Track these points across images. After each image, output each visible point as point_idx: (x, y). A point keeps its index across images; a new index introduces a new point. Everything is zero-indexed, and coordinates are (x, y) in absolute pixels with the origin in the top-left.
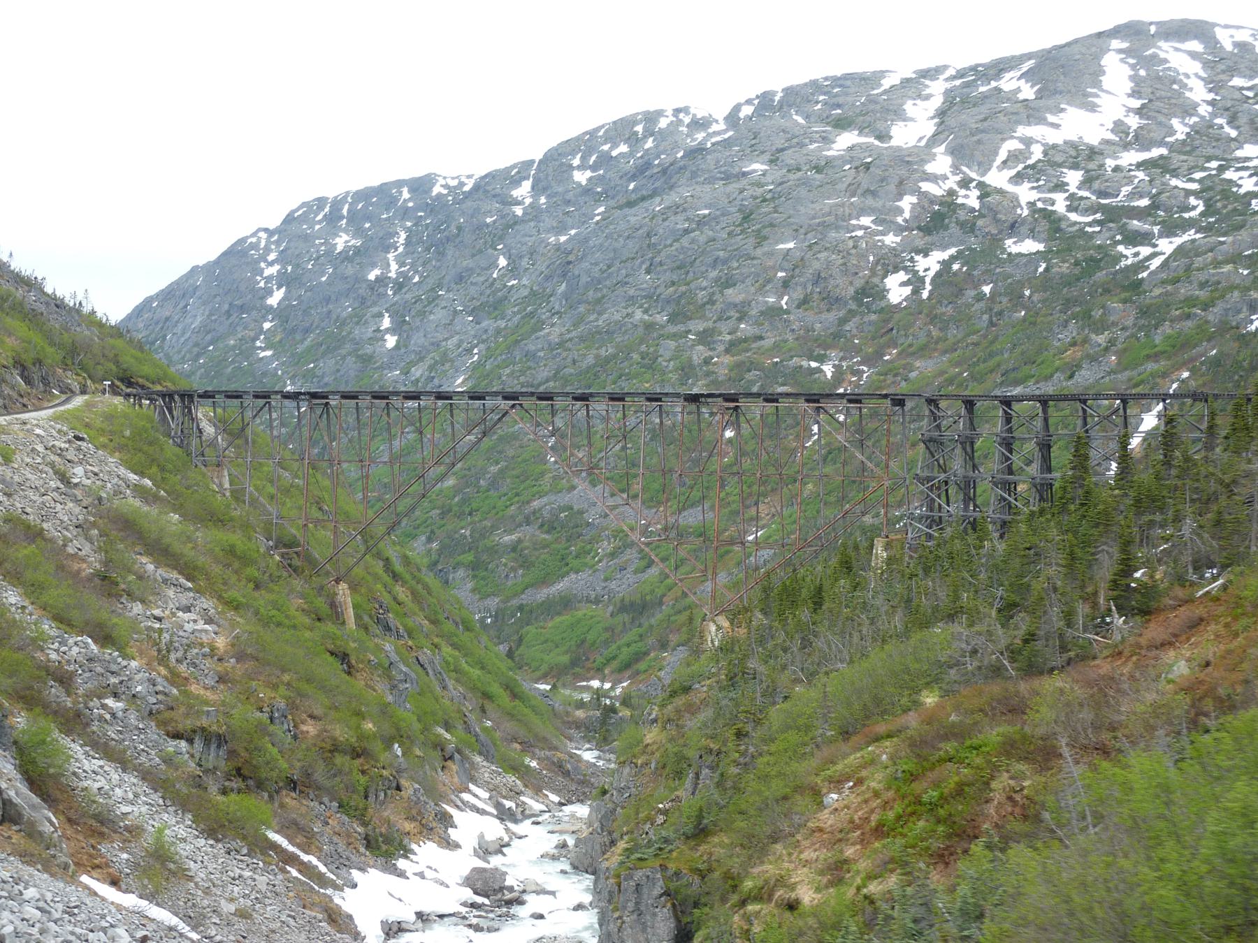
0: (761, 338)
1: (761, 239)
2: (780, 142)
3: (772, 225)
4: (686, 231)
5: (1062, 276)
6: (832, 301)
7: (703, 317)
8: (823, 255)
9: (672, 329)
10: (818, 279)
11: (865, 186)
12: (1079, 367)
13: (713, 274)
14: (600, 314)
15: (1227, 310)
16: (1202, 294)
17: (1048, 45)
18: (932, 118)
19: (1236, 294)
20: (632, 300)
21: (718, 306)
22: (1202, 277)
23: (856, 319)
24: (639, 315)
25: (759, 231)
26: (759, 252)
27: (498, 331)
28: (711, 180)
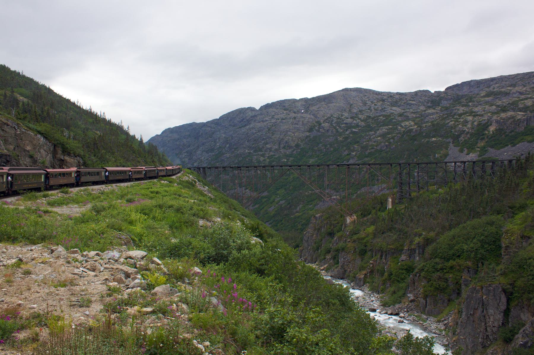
0: (275, 155)
1: (273, 134)
2: (273, 114)
3: (275, 131)
4: (256, 133)
5: (341, 140)
6: (290, 147)
7: (261, 151)
8: (287, 137)
9: (254, 154)
10: (286, 142)
11: (295, 122)
12: (350, 160)
13: (263, 142)
14: (238, 151)
15: (381, 147)
16: (375, 144)
17: (283, 99)
18: (141, 139)
19: (383, 143)
20: (245, 148)
21: (265, 149)
22: (374, 140)
23: (296, 151)
24: (247, 151)
25: (272, 132)
26: (273, 137)
27: (213, 155)
28: (259, 122)
